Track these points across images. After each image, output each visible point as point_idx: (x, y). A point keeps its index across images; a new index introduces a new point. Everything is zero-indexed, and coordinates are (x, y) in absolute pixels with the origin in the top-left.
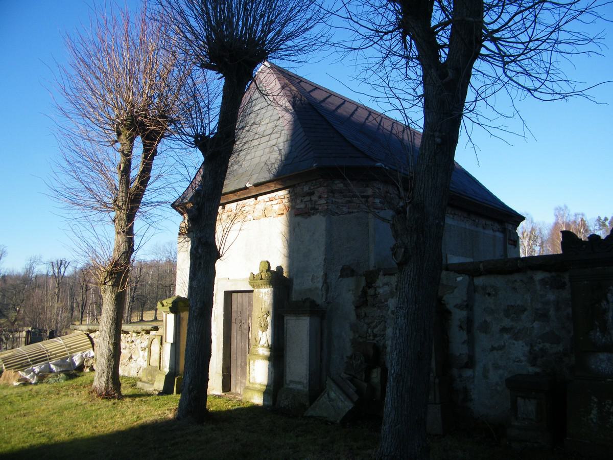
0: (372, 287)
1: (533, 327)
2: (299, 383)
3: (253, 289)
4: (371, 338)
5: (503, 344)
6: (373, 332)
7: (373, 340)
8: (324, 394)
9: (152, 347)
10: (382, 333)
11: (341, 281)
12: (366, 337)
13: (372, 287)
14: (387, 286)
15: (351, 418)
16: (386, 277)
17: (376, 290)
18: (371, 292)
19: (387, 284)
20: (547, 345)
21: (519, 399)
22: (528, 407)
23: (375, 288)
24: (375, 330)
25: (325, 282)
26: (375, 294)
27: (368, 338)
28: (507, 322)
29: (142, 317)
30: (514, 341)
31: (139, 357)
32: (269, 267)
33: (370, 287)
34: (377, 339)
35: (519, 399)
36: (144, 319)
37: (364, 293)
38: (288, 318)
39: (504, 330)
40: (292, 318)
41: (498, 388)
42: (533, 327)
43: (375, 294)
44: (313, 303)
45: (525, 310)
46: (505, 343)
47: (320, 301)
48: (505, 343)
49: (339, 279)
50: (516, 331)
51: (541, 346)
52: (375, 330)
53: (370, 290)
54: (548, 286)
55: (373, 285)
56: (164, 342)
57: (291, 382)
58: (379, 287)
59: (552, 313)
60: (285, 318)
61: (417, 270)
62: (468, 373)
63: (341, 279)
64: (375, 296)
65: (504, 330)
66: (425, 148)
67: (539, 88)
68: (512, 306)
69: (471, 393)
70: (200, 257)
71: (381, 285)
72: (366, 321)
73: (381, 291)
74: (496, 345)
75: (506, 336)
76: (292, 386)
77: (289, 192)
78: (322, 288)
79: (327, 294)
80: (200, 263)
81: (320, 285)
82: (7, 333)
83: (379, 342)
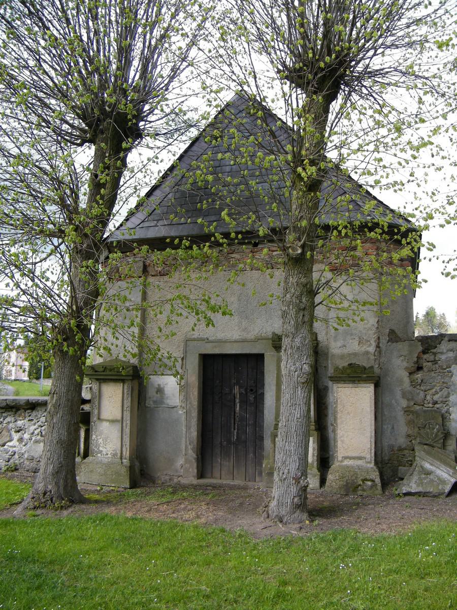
2: (360, 458)
4: (430, 405)
10: (445, 400)
14: (452, 352)
16: (451, 342)
24: (436, 398)
25: (378, 346)
31: (11, 440)
43: (435, 360)
57: (346, 458)
64: (435, 362)
70: (304, 309)
71: (445, 351)
76: (346, 463)
81: (372, 349)
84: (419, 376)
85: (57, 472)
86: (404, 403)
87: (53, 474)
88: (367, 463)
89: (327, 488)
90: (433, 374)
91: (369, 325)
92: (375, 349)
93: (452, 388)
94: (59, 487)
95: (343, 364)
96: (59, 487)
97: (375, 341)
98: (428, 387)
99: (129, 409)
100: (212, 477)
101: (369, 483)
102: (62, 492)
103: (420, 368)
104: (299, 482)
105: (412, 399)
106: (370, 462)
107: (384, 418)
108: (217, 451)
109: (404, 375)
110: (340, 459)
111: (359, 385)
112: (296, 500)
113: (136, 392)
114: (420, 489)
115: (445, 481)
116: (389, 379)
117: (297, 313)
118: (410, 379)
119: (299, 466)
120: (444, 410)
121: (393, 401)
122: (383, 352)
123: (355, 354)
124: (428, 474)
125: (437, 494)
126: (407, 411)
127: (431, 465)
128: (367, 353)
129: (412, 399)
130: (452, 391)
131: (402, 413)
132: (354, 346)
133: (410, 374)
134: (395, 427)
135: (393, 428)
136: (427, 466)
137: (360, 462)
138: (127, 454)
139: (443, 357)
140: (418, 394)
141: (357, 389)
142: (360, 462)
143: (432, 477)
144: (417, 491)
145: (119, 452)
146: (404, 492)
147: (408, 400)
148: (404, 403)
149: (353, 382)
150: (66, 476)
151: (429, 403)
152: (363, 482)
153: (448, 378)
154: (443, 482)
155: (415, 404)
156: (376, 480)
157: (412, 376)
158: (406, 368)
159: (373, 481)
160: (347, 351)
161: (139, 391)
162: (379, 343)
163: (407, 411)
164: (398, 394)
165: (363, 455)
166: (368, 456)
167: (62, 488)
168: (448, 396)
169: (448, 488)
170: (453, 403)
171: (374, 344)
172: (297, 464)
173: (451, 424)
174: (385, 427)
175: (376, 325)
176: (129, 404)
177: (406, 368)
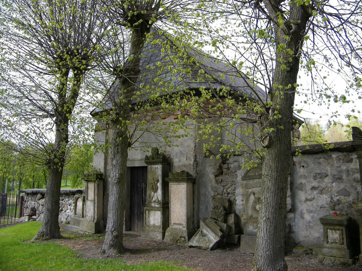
0: (226, 163)
1: (332, 186)
2: (180, 224)
3: (147, 165)
4: (226, 195)
5: (313, 197)
6: (227, 191)
7: (227, 196)
8: (198, 232)
9: (78, 203)
10: (233, 192)
11: (205, 160)
12: (222, 195)
13: (226, 163)
14: (236, 163)
15: (218, 246)
16: (235, 157)
17: (228, 165)
18: (225, 166)
19: (236, 161)
20: (343, 197)
21: (328, 230)
22: (335, 235)
23: (228, 164)
24: (228, 190)
25: (195, 161)
26: (228, 168)
27: (224, 195)
28: (315, 184)
29: (66, 184)
30: (320, 195)
31: (68, 210)
32: (158, 151)
33: (224, 164)
34: (229, 195)
35: (328, 230)
36: (67, 185)
37: (220, 167)
38: (172, 183)
39: (313, 188)
40: (174, 183)
41: (311, 224)
42: (332, 186)
43: (228, 168)
44: (188, 174)
45: (327, 176)
46: (314, 196)
47: (192, 172)
48: (314, 196)
49: (204, 158)
50: (322, 189)
51: (338, 198)
52: (228, 190)
53: (225, 165)
54: (341, 161)
55: (227, 162)
56: (86, 199)
57: (174, 224)
58: (231, 163)
59: (344, 177)
60: (170, 184)
61: (277, 151)
62: (291, 215)
63: (205, 158)
64: (228, 169)
65: (313, 188)
66: (334, 49)
67: (253, 64)
68: (318, 173)
69: (293, 228)
70: (118, 145)
71: (232, 162)
72: (222, 184)
73: (232, 166)
74: (309, 197)
75: (315, 192)
76: (175, 226)
77: (51, 145)
78: (193, 164)
79: (196, 168)
80: (118, 149)
81: (192, 162)
82: (23, 266)
83: (231, 197)
84: (220, 178)
85: (47, 224)
86: (212, 193)
87: (45, 224)
88: (184, 229)
89: (165, 240)
90: (227, 176)
91: (190, 149)
92: (193, 162)
93: (237, 184)
94: (47, 230)
95: (179, 171)
96: (47, 230)
97: (194, 158)
98: (225, 184)
99: (97, 195)
100: (134, 231)
101: (183, 239)
102: (48, 232)
103: (221, 173)
104: (113, 234)
105: (216, 191)
106: (185, 227)
107: (201, 202)
108: (136, 217)
109: (212, 176)
110: (172, 224)
111: (180, 183)
112: (111, 242)
113: (101, 187)
114: (197, 244)
115: (211, 241)
116: (204, 179)
117: (115, 147)
118: (215, 179)
119: (113, 225)
120: (232, 199)
121: (207, 192)
122: (200, 164)
123: (185, 166)
124: (203, 236)
125: (205, 248)
126: (214, 198)
127: (207, 231)
128: (190, 164)
129: (216, 191)
130: (237, 186)
131: (212, 199)
132: (184, 161)
133: (216, 176)
134: (208, 207)
135: (207, 208)
136: (205, 231)
137: (180, 227)
138: (96, 217)
139: (232, 166)
140: (220, 188)
141: (179, 186)
142: (180, 227)
143: (205, 238)
144: (195, 245)
145: (93, 215)
146: (189, 245)
147: (214, 192)
148: (212, 193)
149: (177, 181)
150: (51, 225)
151: (225, 194)
152: (180, 238)
153: (235, 179)
154: (210, 241)
155: (218, 194)
156: (186, 237)
157: (217, 178)
158: (213, 173)
159: (184, 238)
160: (181, 164)
161: (104, 186)
162: (196, 159)
163: (214, 198)
164: (210, 189)
165: (182, 222)
166: (184, 224)
167: (49, 231)
168: (235, 190)
169: (211, 245)
170: (237, 194)
171: (193, 159)
172: (112, 224)
173: (236, 207)
174: (201, 207)
175: (194, 149)
176: (97, 192)
177: (213, 173)
